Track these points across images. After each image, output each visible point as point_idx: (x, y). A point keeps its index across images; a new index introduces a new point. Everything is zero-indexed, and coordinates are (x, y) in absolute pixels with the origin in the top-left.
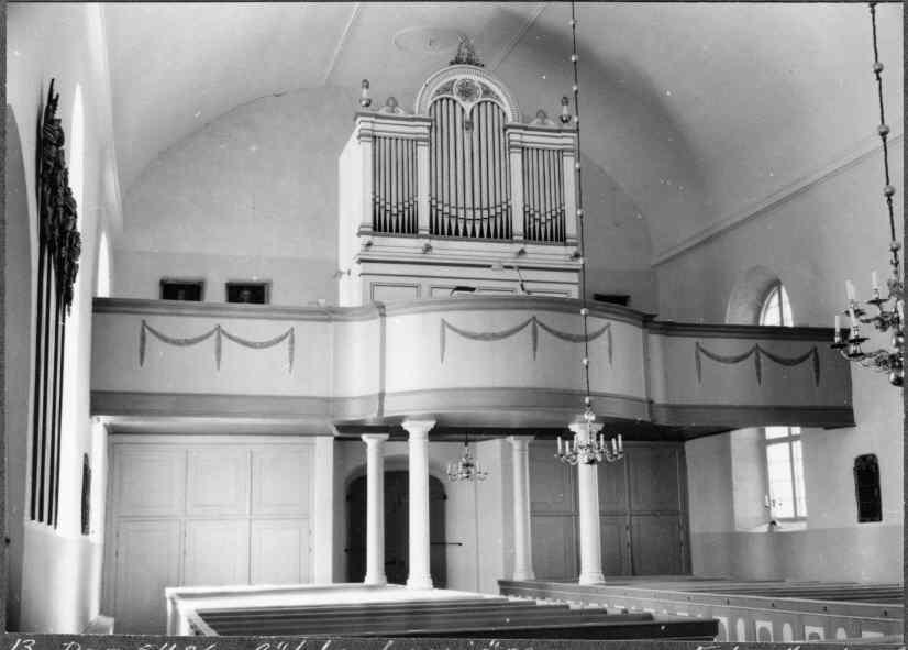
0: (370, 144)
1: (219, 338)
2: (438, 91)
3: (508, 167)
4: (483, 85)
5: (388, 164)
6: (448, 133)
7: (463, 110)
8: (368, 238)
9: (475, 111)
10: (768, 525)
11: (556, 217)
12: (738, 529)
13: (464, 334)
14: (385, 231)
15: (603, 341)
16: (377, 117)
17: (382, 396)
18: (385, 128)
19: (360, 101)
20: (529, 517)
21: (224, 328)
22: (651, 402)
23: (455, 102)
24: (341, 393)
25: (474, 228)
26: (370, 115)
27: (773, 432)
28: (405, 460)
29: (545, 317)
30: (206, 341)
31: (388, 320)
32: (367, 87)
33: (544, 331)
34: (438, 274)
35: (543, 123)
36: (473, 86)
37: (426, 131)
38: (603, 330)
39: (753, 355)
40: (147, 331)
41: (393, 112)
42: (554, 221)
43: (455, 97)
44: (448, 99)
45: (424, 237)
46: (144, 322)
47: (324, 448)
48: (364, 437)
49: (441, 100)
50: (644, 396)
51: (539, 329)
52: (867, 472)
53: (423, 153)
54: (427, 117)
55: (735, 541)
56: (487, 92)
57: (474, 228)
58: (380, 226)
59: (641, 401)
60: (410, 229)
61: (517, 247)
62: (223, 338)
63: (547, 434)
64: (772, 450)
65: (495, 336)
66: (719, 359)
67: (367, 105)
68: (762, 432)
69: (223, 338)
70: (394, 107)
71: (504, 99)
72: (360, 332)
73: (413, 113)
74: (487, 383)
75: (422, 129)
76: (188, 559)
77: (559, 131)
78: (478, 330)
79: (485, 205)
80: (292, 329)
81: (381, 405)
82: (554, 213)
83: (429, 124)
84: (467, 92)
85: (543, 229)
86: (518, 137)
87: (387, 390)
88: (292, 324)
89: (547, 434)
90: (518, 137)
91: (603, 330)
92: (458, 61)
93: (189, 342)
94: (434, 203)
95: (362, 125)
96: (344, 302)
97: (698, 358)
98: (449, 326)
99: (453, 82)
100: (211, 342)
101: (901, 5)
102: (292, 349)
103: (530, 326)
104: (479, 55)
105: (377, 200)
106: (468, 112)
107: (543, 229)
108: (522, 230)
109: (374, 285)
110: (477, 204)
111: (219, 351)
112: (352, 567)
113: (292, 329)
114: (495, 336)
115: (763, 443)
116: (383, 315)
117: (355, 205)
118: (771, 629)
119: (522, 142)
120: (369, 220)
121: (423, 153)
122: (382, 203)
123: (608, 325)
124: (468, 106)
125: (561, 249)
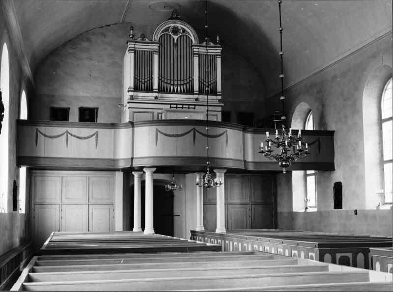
1: (67, 136)
2: (163, 31)
3: (193, 63)
5: (142, 62)
7: (174, 39)
8: (132, 93)
9: (179, 38)
10: (304, 209)
12: (294, 210)
13: (166, 135)
15: (223, 137)
16: (136, 42)
17: (132, 159)
18: (140, 47)
19: (130, 36)
20: (202, 205)
21: (69, 131)
22: (245, 161)
23: (170, 35)
24: (117, 157)
25: (177, 89)
26: (133, 42)
27: (309, 172)
31: (135, 128)
32: (132, 30)
33: (198, 134)
36: (178, 29)
37: (157, 47)
40: (38, 133)
41: (143, 40)
42: (212, 85)
43: (171, 34)
44: (167, 34)
45: (156, 92)
46: (37, 129)
47: (119, 177)
48: (133, 173)
49: (164, 34)
50: (242, 159)
52: (338, 188)
53: (156, 57)
54: (158, 42)
55: (293, 216)
56: (184, 31)
57: (177, 89)
58: (136, 88)
59: (241, 161)
60: (150, 89)
61: (196, 96)
62: (69, 135)
64: (308, 178)
65: (178, 136)
67: (132, 37)
68: (306, 173)
69: (69, 135)
70: (143, 38)
71: (192, 35)
72: (124, 134)
73: (152, 40)
74: (175, 154)
75: (156, 47)
76: (63, 221)
77: (215, 47)
78: (171, 133)
79: (182, 79)
80: (97, 132)
81: (132, 162)
82: (212, 82)
83: (158, 45)
84: (175, 31)
85: (143, 85)
86: (197, 50)
87: (134, 157)
88: (96, 130)
90: (197, 50)
92: (172, 18)
93: (56, 137)
94: (160, 78)
95: (131, 45)
98: (159, 131)
99: (169, 27)
100: (64, 137)
101: (26, 119)
102: (97, 140)
103: (192, 132)
105: (136, 77)
106: (176, 40)
107: (143, 85)
109: (134, 112)
110: (179, 79)
111: (67, 140)
112: (129, 225)
113: (97, 132)
114: (178, 136)
115: (306, 176)
116: (133, 127)
117: (129, 81)
118: (297, 254)
119: (198, 52)
120: (132, 85)
121: (156, 57)
122: (138, 78)
123: (227, 131)
124: (176, 37)
125: (214, 97)
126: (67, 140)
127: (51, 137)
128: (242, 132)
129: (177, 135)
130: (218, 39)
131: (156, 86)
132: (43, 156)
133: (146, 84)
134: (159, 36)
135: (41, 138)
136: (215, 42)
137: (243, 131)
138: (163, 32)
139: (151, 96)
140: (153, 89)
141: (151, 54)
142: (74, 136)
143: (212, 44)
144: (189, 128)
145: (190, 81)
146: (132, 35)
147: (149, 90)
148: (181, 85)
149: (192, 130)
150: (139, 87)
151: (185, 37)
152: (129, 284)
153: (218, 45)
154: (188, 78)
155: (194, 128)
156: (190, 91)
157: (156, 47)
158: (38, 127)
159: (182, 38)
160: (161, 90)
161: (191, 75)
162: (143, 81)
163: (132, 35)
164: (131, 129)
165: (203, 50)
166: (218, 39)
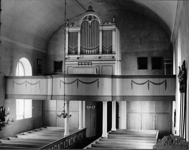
0: (102, 32)
1: (26, 83)
4: (94, 16)
6: (96, 27)
11: (111, 47)
14: (104, 53)
25: (89, 51)
28: (64, 130)
29: (80, 79)
30: (145, 84)
31: (54, 79)
33: (80, 82)
34: (104, 64)
35: (108, 24)
38: (97, 80)
39: (147, 83)
42: (76, 49)
43: (87, 20)
49: (84, 21)
51: (79, 81)
56: (95, 18)
57: (89, 51)
58: (69, 53)
60: (76, 53)
62: (27, 83)
63: (140, 113)
66: (137, 84)
67: (67, 25)
69: (27, 83)
70: (73, 25)
71: (87, 15)
73: (77, 25)
77: (111, 25)
84: (90, 18)
85: (107, 50)
89: (140, 113)
90: (101, 28)
91: (97, 80)
96: (116, 74)
97: (132, 84)
99: (87, 16)
103: (77, 81)
104: (94, 9)
106: (90, 23)
107: (107, 50)
108: (80, 52)
111: (26, 85)
124: (90, 22)
126: (26, 85)
127: (19, 84)
128: (111, 79)
129: (69, 83)
130: (114, 20)
131: (79, 51)
132: (16, 94)
133: (76, 49)
134: (81, 22)
135: (15, 85)
136: (112, 22)
137: (112, 78)
138: (84, 19)
139: (76, 56)
140: (112, 52)
141: (77, 33)
142: (29, 83)
143: (110, 23)
144: (75, 79)
145: (108, 48)
146: (67, 24)
147: (98, 53)
148: (93, 49)
149: (76, 80)
150: (71, 52)
151: (96, 21)
152: (151, 86)
153: (113, 24)
154: (109, 45)
155: (78, 79)
156: (98, 53)
157: (79, 29)
158: (14, 79)
159: (94, 21)
160: (82, 53)
161: (98, 43)
162: (107, 47)
163: (67, 24)
164: (51, 79)
165: (105, 28)
166: (114, 20)
